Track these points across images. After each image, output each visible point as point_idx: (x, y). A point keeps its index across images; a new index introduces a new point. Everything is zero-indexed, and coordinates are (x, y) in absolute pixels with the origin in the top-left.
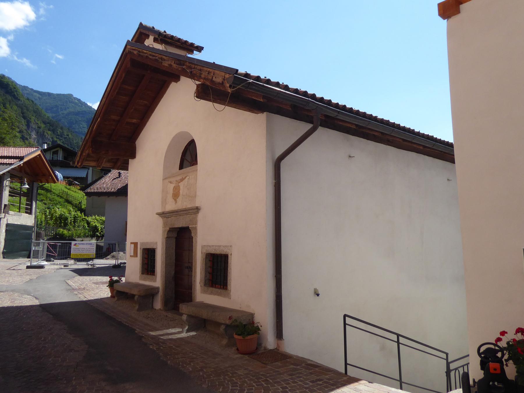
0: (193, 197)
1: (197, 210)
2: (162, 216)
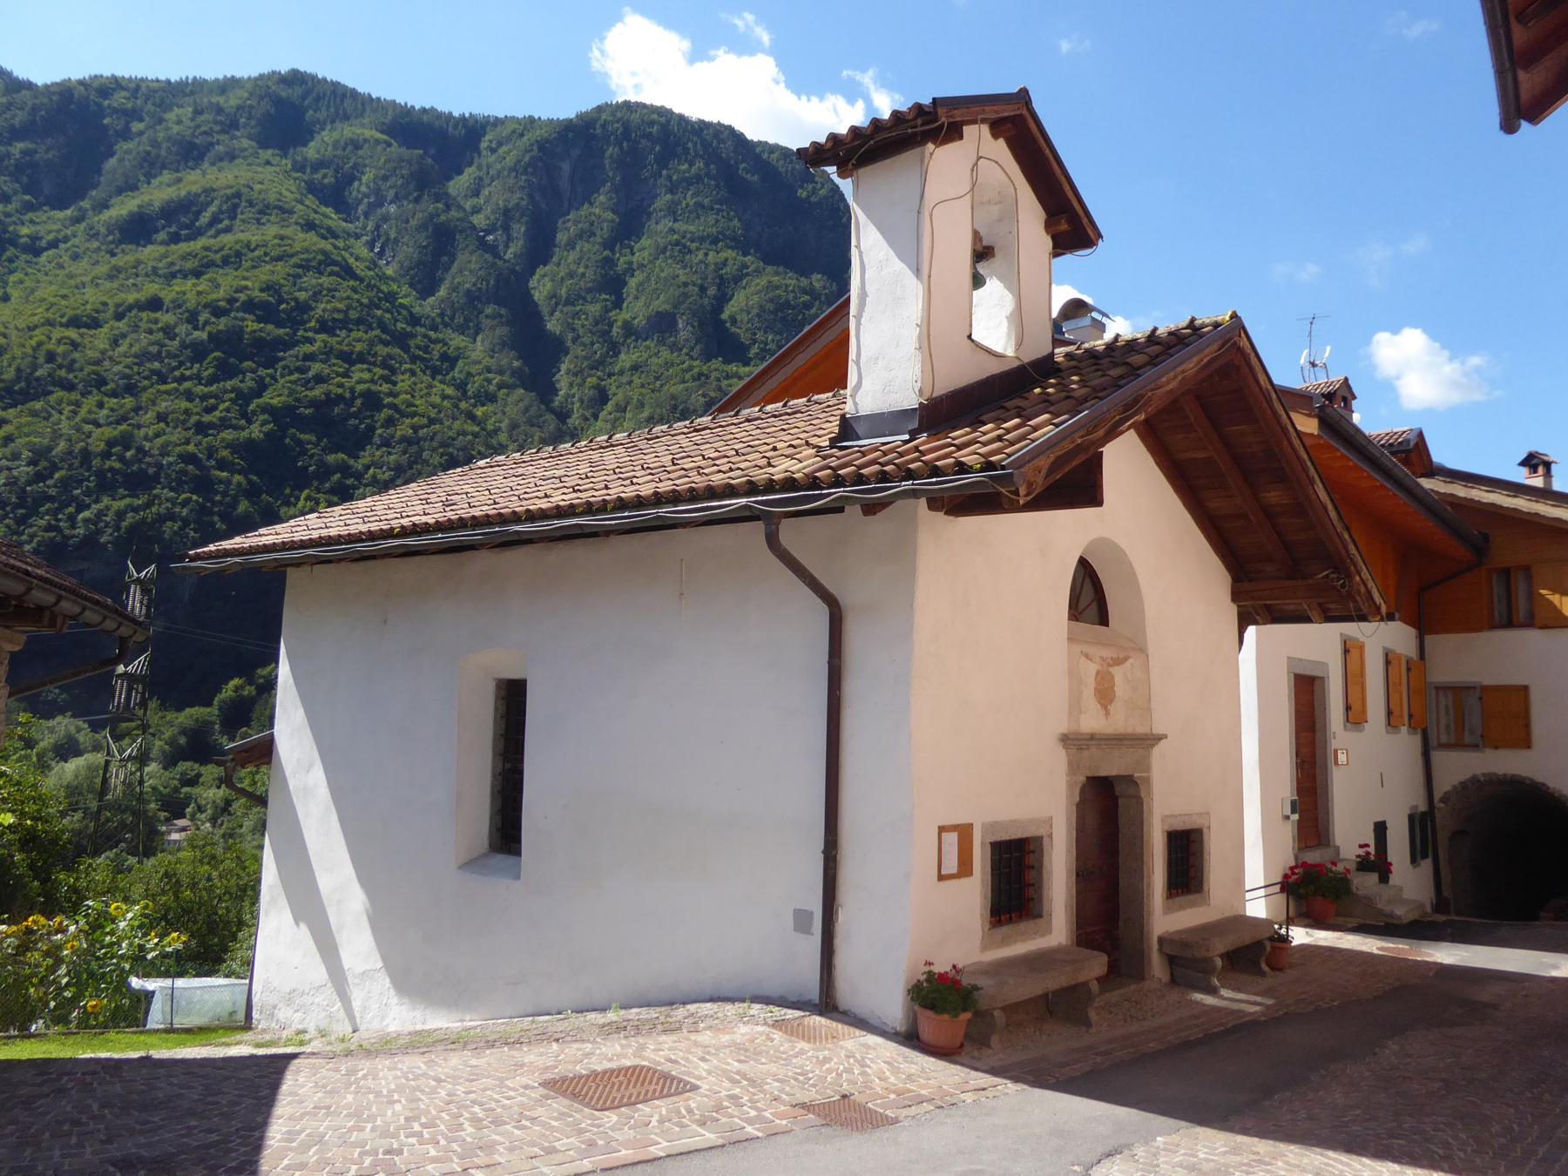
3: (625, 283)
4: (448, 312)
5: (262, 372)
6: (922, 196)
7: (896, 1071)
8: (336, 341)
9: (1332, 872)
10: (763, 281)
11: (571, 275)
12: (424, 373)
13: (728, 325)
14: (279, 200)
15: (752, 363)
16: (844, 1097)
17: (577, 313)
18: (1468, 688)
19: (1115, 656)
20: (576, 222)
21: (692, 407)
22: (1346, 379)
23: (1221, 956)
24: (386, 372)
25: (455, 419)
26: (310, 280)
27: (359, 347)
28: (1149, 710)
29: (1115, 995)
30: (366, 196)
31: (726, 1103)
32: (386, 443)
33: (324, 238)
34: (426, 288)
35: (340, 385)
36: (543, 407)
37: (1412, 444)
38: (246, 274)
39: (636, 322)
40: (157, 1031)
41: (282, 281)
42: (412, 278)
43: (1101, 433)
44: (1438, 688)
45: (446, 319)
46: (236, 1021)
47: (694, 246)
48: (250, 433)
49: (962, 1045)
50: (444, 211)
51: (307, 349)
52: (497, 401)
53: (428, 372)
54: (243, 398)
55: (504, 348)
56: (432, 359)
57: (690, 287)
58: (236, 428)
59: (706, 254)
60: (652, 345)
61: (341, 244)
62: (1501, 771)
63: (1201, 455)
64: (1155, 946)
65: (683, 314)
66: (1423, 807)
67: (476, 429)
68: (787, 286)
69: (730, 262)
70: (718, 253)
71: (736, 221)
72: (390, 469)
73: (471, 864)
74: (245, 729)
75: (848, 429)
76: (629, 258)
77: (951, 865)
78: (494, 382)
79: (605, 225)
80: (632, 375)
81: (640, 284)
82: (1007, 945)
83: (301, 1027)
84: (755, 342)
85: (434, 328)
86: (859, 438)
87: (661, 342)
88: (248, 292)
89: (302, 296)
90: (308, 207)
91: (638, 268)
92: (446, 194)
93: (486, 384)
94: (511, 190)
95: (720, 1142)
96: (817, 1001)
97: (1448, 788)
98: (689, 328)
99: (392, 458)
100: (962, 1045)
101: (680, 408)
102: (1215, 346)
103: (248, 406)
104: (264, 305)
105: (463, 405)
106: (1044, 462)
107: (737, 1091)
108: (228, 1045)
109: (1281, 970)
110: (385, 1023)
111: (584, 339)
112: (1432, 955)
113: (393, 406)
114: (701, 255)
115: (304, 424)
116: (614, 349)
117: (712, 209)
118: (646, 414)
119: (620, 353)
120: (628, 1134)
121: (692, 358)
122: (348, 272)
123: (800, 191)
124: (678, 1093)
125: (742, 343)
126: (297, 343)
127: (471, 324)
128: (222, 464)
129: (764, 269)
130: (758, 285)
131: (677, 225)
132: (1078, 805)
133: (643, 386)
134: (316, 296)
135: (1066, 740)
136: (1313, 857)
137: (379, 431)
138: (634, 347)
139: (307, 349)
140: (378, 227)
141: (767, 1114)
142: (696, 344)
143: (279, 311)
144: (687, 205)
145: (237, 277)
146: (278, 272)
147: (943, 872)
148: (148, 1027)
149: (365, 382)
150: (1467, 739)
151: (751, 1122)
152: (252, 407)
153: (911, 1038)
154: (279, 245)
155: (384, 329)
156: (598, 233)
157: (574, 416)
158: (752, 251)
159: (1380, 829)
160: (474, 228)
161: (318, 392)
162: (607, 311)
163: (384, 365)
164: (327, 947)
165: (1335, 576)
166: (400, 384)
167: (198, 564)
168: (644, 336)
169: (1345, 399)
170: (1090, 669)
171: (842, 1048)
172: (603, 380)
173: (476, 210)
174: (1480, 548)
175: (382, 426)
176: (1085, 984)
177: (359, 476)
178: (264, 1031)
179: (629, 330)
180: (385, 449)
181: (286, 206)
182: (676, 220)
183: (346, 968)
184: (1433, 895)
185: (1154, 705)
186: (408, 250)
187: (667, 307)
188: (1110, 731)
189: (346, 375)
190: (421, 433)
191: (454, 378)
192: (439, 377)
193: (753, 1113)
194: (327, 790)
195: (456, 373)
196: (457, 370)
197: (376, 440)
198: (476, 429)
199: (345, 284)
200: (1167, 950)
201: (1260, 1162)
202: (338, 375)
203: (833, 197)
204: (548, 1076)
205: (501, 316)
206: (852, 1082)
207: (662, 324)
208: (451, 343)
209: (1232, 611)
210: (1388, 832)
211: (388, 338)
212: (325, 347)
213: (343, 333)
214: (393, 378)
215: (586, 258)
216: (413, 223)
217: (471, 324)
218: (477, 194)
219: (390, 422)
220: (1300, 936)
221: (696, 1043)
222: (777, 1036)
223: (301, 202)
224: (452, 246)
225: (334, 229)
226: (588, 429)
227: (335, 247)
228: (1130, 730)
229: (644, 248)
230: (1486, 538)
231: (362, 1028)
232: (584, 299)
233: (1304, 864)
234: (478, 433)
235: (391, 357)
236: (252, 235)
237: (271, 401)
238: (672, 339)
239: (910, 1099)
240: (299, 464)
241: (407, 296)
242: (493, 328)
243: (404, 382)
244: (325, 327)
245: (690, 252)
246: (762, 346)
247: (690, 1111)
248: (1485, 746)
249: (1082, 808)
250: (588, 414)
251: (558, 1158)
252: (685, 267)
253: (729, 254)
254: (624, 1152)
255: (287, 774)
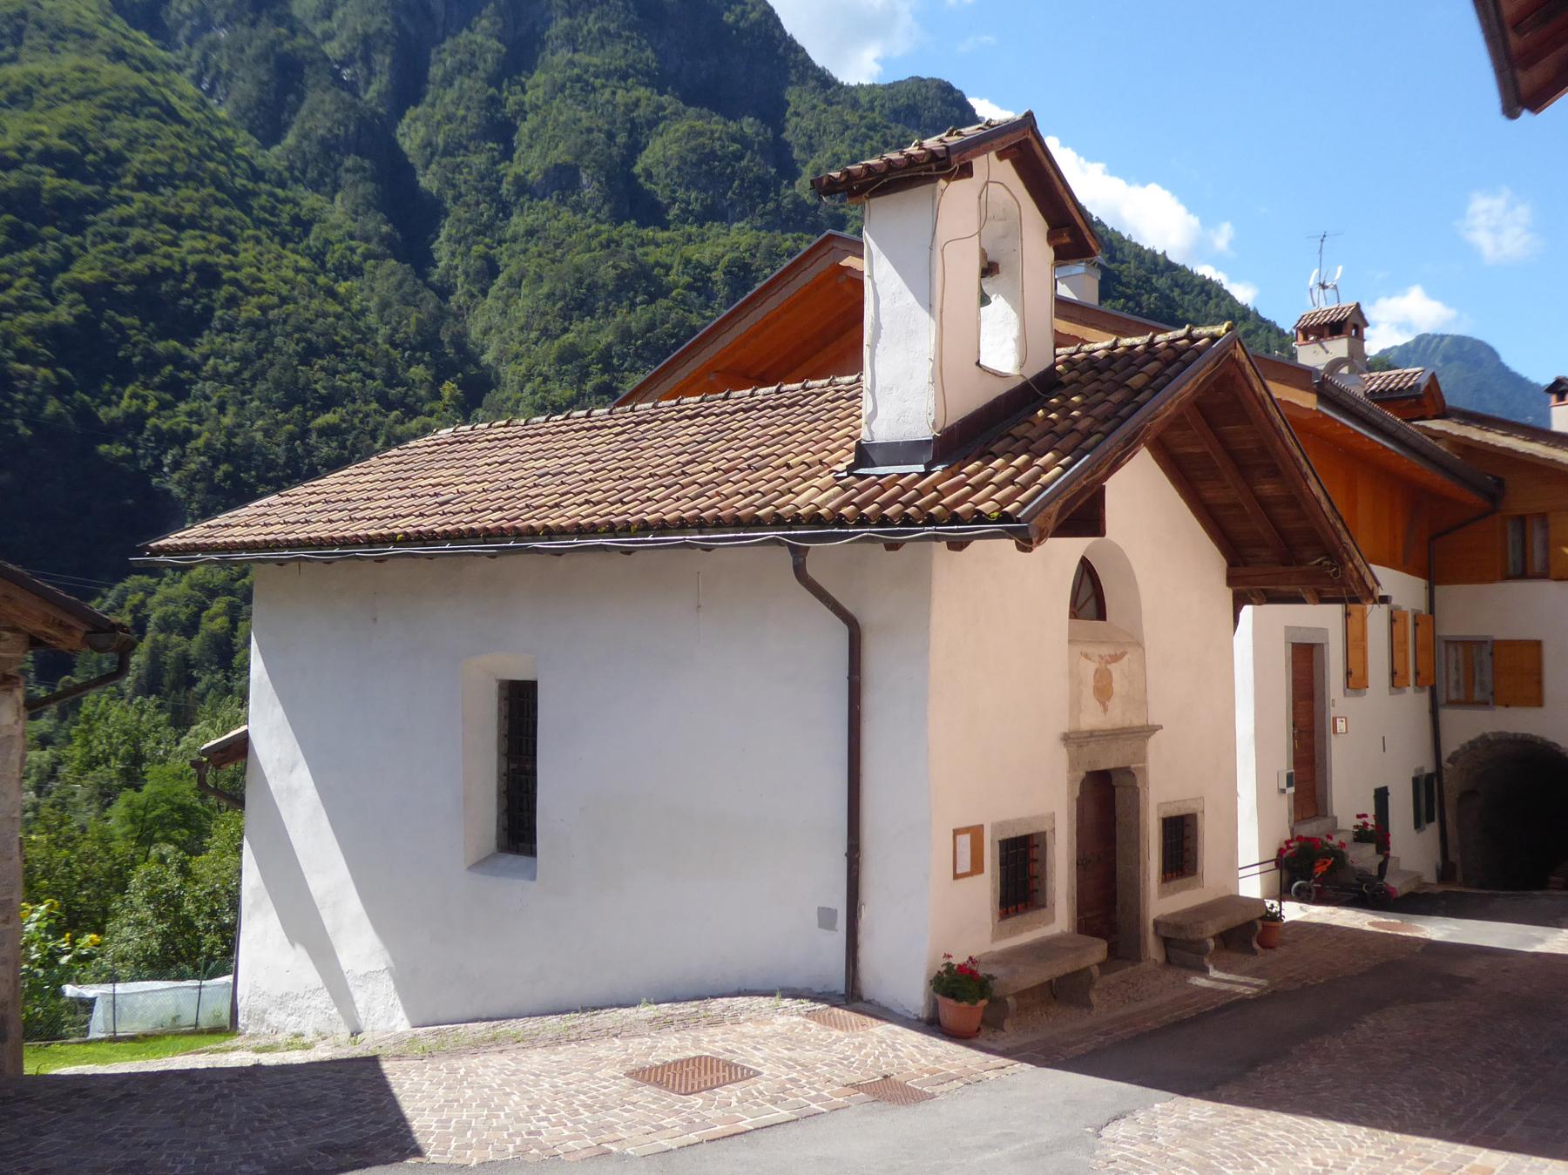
0: (1142, 703)
1: (1151, 730)
2: (1437, 340)
3: (515, 129)
4: (298, 164)
5: (68, 240)
6: (934, 233)
7: (924, 1054)
8: (165, 200)
9: (1327, 845)
10: (682, 127)
11: (449, 118)
12: (272, 241)
13: (642, 180)
14: (78, 22)
15: (672, 227)
16: (886, 1077)
17: (458, 166)
18: (1479, 643)
19: (1112, 653)
20: (453, 53)
21: (600, 282)
22: (1358, 305)
23: (1214, 937)
24: (225, 240)
25: (311, 296)
26: (121, 124)
27: (189, 209)
28: (1146, 703)
29: (1112, 978)
30: (189, 17)
31: (788, 1086)
32: (229, 327)
33: (138, 70)
34: (270, 133)
35: (168, 256)
36: (419, 282)
37: (1422, 388)
38: (41, 116)
39: (530, 177)
40: (101, 1040)
41: (87, 126)
42: (252, 121)
43: (1104, 471)
44: (1448, 642)
45: (297, 173)
46: (179, 1026)
47: (598, 82)
48: (56, 317)
49: (979, 1029)
50: (288, 38)
51: (124, 211)
52: (363, 275)
53: (277, 239)
54: (44, 273)
55: (369, 209)
56: (280, 223)
57: (596, 134)
58: (37, 309)
59: (614, 93)
60: (551, 205)
61: (159, 78)
62: (1511, 730)
63: (1198, 450)
64: (1151, 928)
65: (587, 167)
66: (1429, 768)
67: (339, 309)
68: (712, 132)
69: (643, 103)
70: (628, 91)
71: (649, 53)
72: (235, 359)
73: (480, 865)
74: (67, 677)
75: (864, 455)
76: (520, 96)
77: (965, 865)
78: (359, 251)
79: (489, 56)
80: (527, 242)
81: (533, 131)
82: (1015, 934)
83: (296, 1030)
84: (674, 200)
85: (282, 184)
86: (874, 465)
87: (561, 201)
88: (44, 139)
89: (114, 144)
90: (114, 31)
91: (531, 110)
92: (290, 16)
93: (348, 253)
94: (371, 12)
95: (794, 1117)
96: (843, 992)
97: (1456, 748)
98: (595, 183)
99: (237, 345)
100: (979, 1029)
101: (587, 281)
102: (1212, 364)
103: (52, 281)
104: (65, 156)
105: (322, 280)
106: (1054, 508)
107: (794, 1075)
108: (225, 1051)
109: (1271, 947)
110: (392, 1024)
111: (468, 199)
112: (1421, 930)
113: (235, 282)
114: (607, 94)
115: (124, 304)
116: (505, 210)
117: (620, 36)
118: (545, 289)
119: (511, 214)
120: (714, 1113)
121: (599, 221)
122: (170, 114)
123: (727, 14)
124: (743, 1079)
125: (660, 202)
126: (108, 204)
127: (327, 180)
128: (23, 355)
129: (684, 112)
130: (677, 130)
131: (577, 57)
132: (1078, 800)
133: (540, 255)
134: (132, 144)
135: (1067, 739)
136: (1309, 829)
137: (219, 313)
138: (529, 208)
139: (124, 211)
140: (205, 57)
141: (825, 1093)
142: (604, 203)
143: (84, 163)
144: (589, 32)
145: (28, 119)
146: (82, 114)
147: (958, 872)
148: (90, 1037)
149: (198, 252)
150: (1477, 696)
151: (814, 1100)
152: (57, 283)
153: (933, 1025)
154: (81, 80)
155: (220, 186)
156: (481, 66)
157: (458, 293)
158: (669, 89)
159: (1381, 796)
160: (326, 59)
161: (139, 264)
162: (495, 163)
163: (223, 231)
164: (321, 951)
165: (1328, 563)
166: (242, 255)
167: (162, 558)
168: (540, 193)
169: (1356, 327)
170: (1089, 668)
171: (873, 1034)
172: (491, 248)
173: (329, 36)
174: (1495, 494)
175: (222, 307)
176: (1087, 969)
177: (196, 368)
178: (253, 1036)
179: (522, 186)
180: (226, 335)
181: (86, 29)
182: (575, 51)
183: (345, 970)
184: (1437, 858)
185: (1150, 697)
186: (245, 87)
187: (568, 158)
188: (1108, 726)
189: (174, 243)
190: (272, 314)
191: (309, 247)
192: (290, 245)
193: (813, 1093)
194: (315, 791)
195: (312, 241)
196: (312, 236)
197: (216, 323)
198: (339, 309)
199: (167, 129)
200: (1162, 932)
201: (1242, 1122)
202: (164, 243)
203: (766, 22)
204: (628, 1068)
205: (364, 170)
206: (887, 1064)
207: (562, 180)
208: (303, 203)
209: (1227, 595)
210: (1390, 798)
211: (225, 197)
212: (147, 208)
213: (168, 192)
214: (234, 247)
215: (466, 97)
216: (250, 52)
217: (327, 180)
218: (328, 16)
219: (232, 302)
220: (1293, 911)
221: (743, 1035)
222: (813, 1025)
223: (106, 25)
224: (300, 81)
225: (150, 59)
226: (475, 308)
227: (153, 82)
228: (1127, 724)
229: (537, 85)
230: (1500, 483)
231: (367, 1028)
232: (466, 148)
233: (1300, 838)
234: (342, 314)
235: (230, 221)
236: (45, 66)
237: (82, 277)
238: (574, 197)
239: (942, 1077)
240: (120, 354)
241: (246, 143)
242: (355, 184)
243: (247, 252)
244: (145, 183)
245: (594, 89)
246: (683, 206)
247: (761, 1093)
248: (1496, 703)
249: (1081, 804)
250: (475, 291)
251: (668, 1133)
252: (588, 109)
253: (642, 92)
254: (719, 1127)
255: (267, 773)
